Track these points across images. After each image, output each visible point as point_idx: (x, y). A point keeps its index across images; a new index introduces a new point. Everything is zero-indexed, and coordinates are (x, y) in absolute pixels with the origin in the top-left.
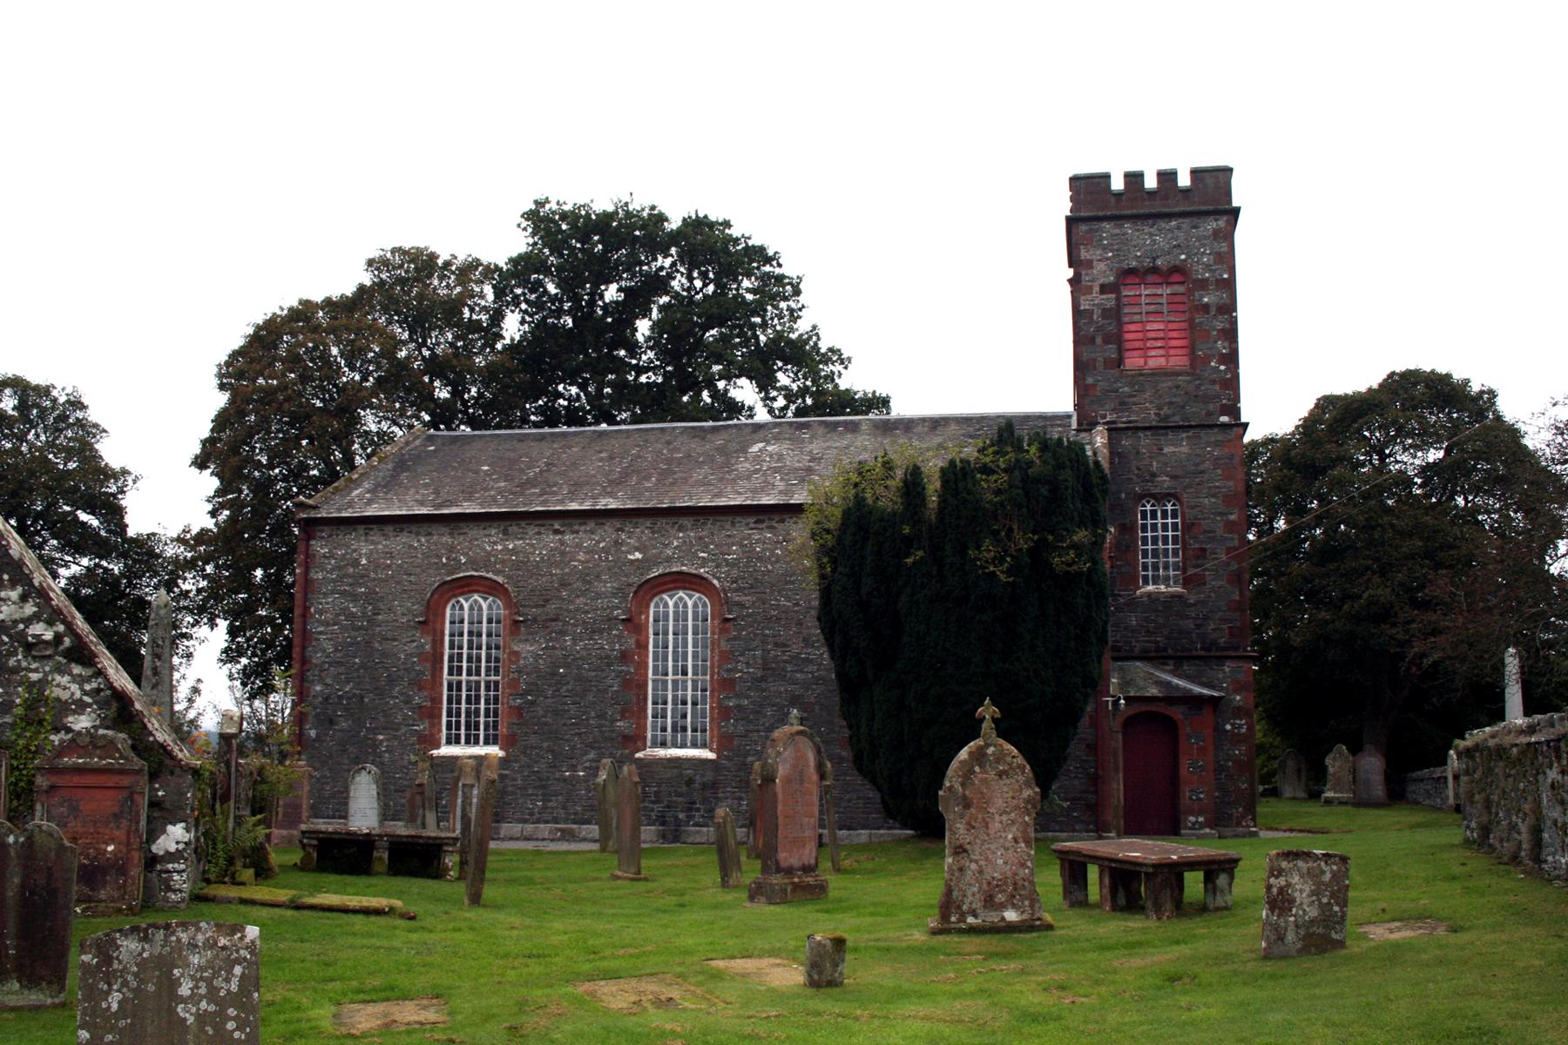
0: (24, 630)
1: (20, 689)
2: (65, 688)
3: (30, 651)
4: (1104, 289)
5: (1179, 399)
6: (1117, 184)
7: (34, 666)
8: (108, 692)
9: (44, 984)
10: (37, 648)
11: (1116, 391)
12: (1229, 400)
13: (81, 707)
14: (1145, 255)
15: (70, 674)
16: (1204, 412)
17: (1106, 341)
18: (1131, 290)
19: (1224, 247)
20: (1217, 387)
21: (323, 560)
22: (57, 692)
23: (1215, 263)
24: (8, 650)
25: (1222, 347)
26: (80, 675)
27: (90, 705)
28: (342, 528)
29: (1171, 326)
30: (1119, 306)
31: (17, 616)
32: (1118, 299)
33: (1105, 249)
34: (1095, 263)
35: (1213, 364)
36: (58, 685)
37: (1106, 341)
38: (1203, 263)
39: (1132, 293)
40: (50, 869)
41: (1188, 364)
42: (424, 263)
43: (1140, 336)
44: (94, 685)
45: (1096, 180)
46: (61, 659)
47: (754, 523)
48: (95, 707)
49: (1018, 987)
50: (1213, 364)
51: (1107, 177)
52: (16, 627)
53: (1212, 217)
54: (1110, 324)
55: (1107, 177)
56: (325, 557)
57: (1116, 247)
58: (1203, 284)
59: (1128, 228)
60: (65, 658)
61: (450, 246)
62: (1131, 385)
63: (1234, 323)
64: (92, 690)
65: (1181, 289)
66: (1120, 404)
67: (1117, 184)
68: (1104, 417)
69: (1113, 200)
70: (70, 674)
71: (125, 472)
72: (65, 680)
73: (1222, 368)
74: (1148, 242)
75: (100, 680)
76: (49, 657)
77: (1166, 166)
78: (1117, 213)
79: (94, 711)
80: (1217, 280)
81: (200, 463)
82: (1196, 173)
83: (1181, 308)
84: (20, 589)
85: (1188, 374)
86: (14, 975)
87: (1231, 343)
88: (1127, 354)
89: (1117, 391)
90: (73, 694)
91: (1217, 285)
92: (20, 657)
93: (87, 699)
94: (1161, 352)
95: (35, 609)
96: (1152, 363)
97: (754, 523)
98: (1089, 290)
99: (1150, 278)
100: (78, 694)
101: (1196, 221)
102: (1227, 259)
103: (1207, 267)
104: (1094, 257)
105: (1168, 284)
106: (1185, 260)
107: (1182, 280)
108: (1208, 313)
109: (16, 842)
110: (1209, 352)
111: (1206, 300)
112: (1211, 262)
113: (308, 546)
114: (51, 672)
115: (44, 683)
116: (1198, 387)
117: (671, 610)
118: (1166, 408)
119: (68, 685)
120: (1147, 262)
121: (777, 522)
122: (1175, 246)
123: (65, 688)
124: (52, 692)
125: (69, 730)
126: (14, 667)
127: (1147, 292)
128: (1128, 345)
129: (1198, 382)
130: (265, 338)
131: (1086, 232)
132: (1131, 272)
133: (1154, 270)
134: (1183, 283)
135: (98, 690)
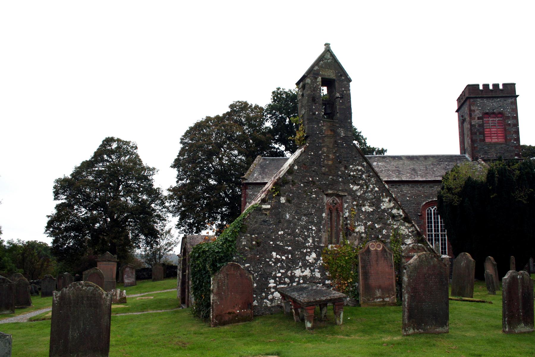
0: (391, 211)
1: (391, 231)
2: (404, 231)
3: (394, 218)
4: (479, 118)
5: (502, 151)
6: (481, 88)
7: (395, 223)
8: (416, 232)
9: (529, 324)
10: (397, 217)
11: (484, 149)
12: (517, 152)
13: (409, 236)
14: (490, 109)
15: (405, 226)
16: (510, 155)
17: (480, 134)
18: (486, 119)
19: (514, 106)
20: (514, 148)
21: (250, 196)
22: (402, 232)
23: (512, 112)
24: (387, 218)
25: (514, 136)
26: (408, 226)
27: (411, 236)
28: (257, 186)
29: (499, 130)
30: (483, 123)
31: (389, 207)
32: (483, 121)
33: (478, 106)
34: (476, 111)
35: (512, 141)
36: (402, 230)
37: (480, 134)
38: (508, 111)
39: (486, 120)
40: (528, 286)
41: (504, 141)
42: (244, 106)
43: (489, 132)
44: (412, 230)
45: (475, 86)
46: (402, 221)
47: (391, 186)
48: (412, 236)
49: (326, 336)
50: (512, 141)
51: (478, 85)
52: (388, 210)
53: (510, 98)
54: (481, 129)
55: (478, 85)
56: (251, 195)
57: (482, 106)
58: (508, 118)
59: (485, 101)
60: (403, 220)
61: (252, 102)
62: (488, 147)
63: (518, 129)
64: (411, 231)
65: (501, 119)
66: (485, 153)
67: (481, 88)
68: (480, 156)
69: (480, 92)
70: (405, 226)
71: (154, 169)
72: (403, 228)
73: (515, 142)
74: (491, 105)
75: (413, 228)
76: (399, 220)
77: (496, 82)
78: (482, 96)
79: (412, 238)
80: (513, 117)
81: (174, 166)
82: (504, 85)
83: (501, 124)
84: (389, 198)
85: (505, 144)
86: (523, 322)
87: (517, 135)
88: (486, 138)
89: (484, 149)
90: (406, 232)
91: (513, 118)
92: (391, 220)
93: (410, 234)
94: (496, 137)
95: (394, 205)
96: (494, 141)
97: (391, 186)
98: (474, 119)
99: (492, 116)
100: (407, 233)
101: (505, 99)
102: (515, 110)
103: (509, 112)
104: (475, 109)
105: (498, 117)
106: (503, 110)
107: (495, 116)
108: (510, 126)
109: (520, 278)
110: (511, 138)
111: (509, 122)
112: (510, 111)
113: (245, 191)
114: (400, 225)
115: (398, 229)
116: (508, 148)
117: (433, 212)
118: (499, 154)
119: (405, 229)
120: (491, 111)
121: (398, 186)
122: (499, 106)
123: (404, 231)
124: (400, 232)
125: (406, 244)
126: (389, 223)
127: (491, 120)
128: (486, 135)
129: (508, 146)
130: (199, 126)
131: (473, 102)
132: (487, 113)
133: (494, 113)
134: (501, 117)
135: (413, 231)
